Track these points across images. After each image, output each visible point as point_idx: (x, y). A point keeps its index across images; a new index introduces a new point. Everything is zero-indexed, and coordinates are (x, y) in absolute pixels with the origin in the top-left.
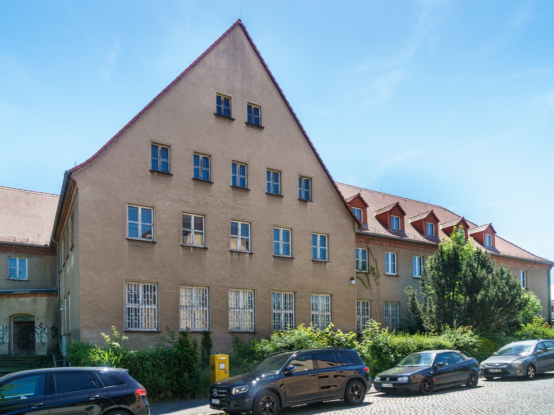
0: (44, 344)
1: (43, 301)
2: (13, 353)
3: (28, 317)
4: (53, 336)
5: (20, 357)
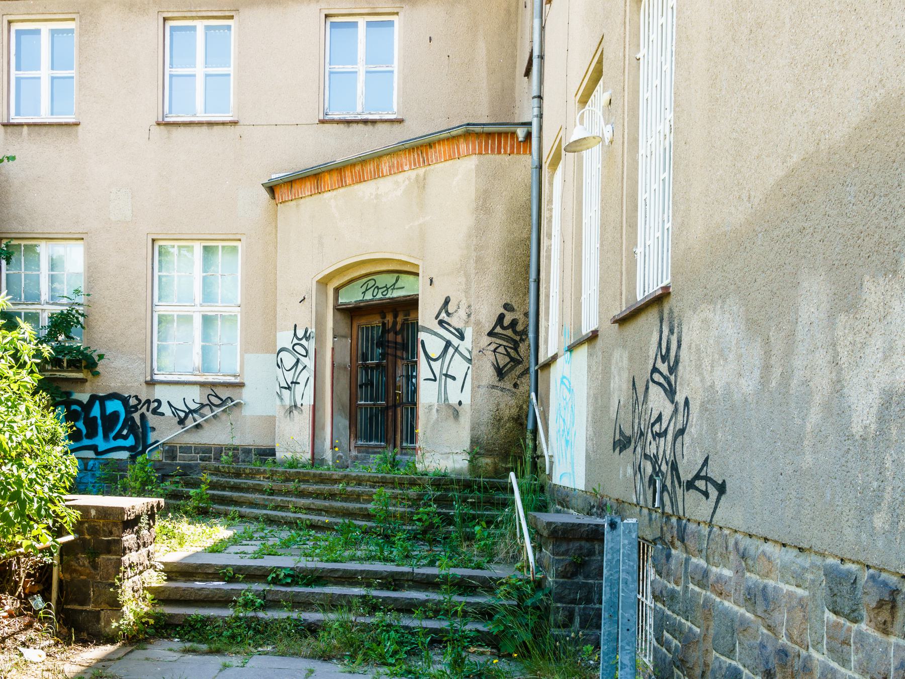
0: (455, 412)
1: (459, 177)
2: (328, 455)
3: (389, 279)
4: (500, 373)
5: (347, 479)
